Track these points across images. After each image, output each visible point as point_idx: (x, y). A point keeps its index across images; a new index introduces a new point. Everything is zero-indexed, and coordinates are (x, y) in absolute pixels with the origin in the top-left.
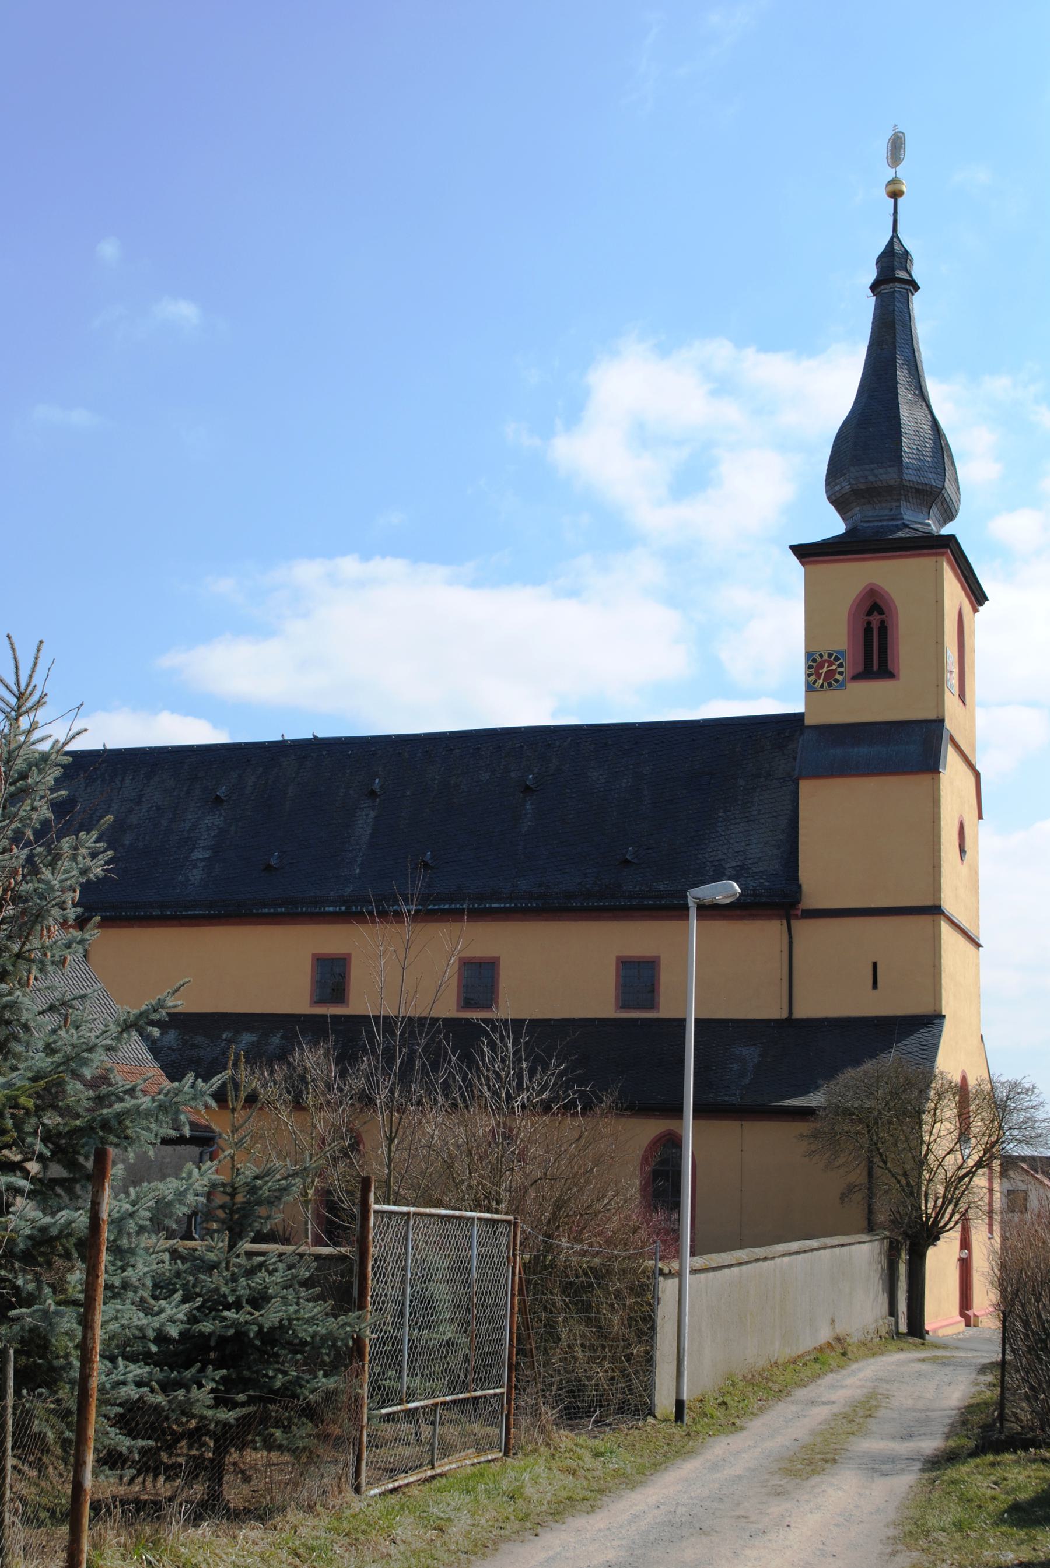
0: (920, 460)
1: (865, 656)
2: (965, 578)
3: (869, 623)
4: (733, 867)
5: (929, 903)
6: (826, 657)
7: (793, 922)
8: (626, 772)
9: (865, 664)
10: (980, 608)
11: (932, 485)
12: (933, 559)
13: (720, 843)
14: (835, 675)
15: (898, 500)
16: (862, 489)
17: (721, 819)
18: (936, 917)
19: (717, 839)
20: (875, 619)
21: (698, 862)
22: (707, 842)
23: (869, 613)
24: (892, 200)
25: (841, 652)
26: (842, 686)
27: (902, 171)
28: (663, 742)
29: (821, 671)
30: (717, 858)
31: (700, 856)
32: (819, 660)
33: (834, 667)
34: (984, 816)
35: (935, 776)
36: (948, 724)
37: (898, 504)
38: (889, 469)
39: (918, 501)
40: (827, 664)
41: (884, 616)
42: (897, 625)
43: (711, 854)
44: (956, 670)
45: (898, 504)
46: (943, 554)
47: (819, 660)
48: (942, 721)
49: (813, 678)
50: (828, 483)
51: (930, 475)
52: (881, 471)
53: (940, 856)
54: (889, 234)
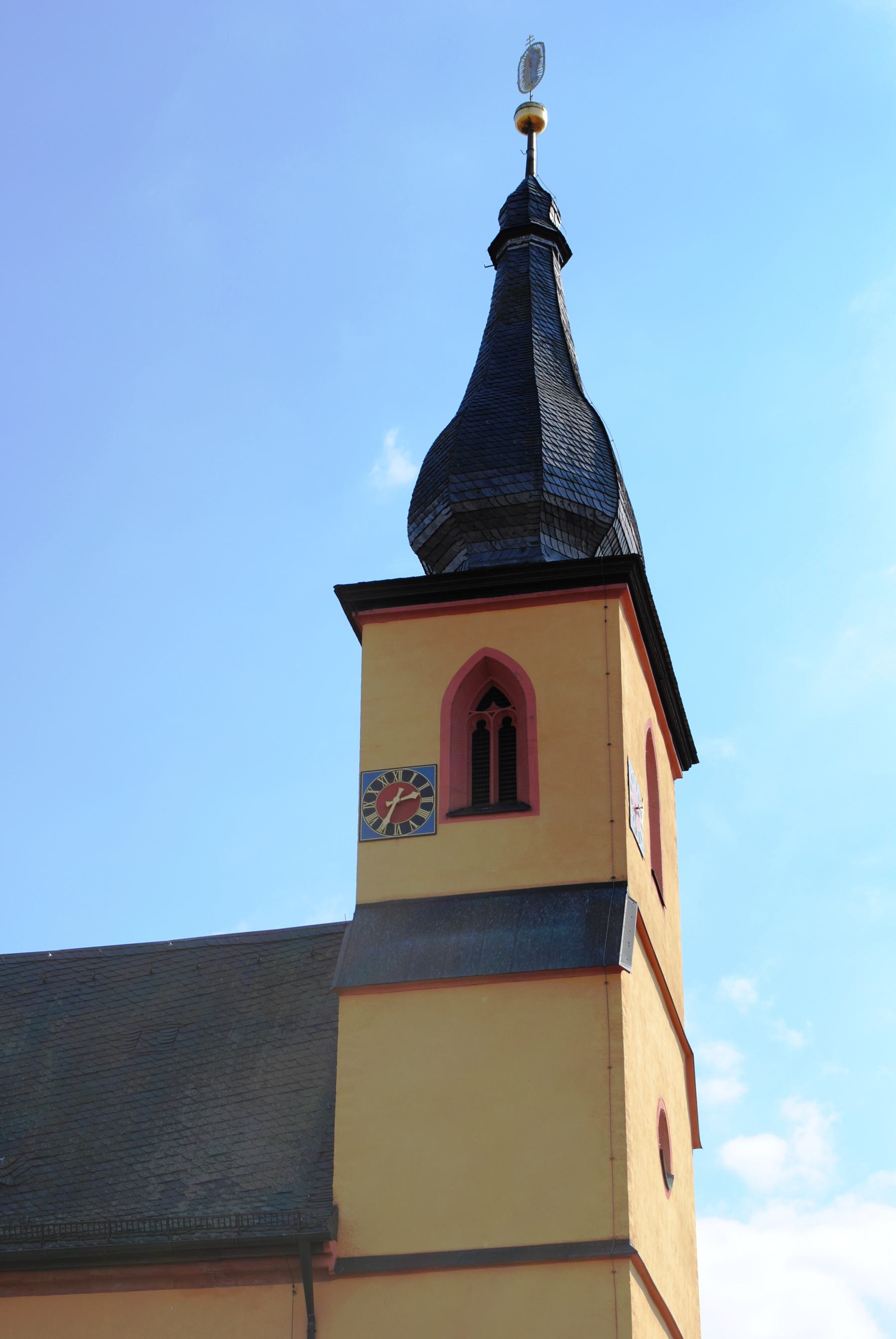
0: (573, 466)
1: (474, 759)
2: (658, 679)
3: (481, 724)
4: (202, 1184)
5: (603, 1233)
6: (399, 779)
7: (319, 1288)
8: (16, 1031)
9: (474, 793)
10: (684, 773)
11: (595, 509)
12: (601, 603)
13: (181, 1142)
14: (416, 810)
15: (536, 532)
16: (470, 512)
17: (188, 1101)
18: (619, 1264)
19: (176, 1135)
20: (493, 716)
21: (133, 1177)
22: (156, 1140)
23: (483, 705)
24: (525, 138)
25: (430, 769)
26: (430, 830)
27: (538, 94)
28: (94, 979)
29: (388, 804)
30: (172, 1169)
31: (138, 1167)
32: (386, 784)
33: (414, 795)
34: (703, 1140)
35: (610, 978)
36: (630, 889)
37: (534, 539)
38: (519, 477)
39: (572, 538)
40: (401, 790)
41: (509, 708)
42: (534, 718)
43: (161, 1162)
44: (644, 812)
45: (534, 539)
46: (616, 594)
47: (386, 784)
48: (623, 885)
49: (374, 816)
50: (413, 518)
51: (592, 493)
52: (505, 480)
53: (623, 1137)
54: (523, 177)
